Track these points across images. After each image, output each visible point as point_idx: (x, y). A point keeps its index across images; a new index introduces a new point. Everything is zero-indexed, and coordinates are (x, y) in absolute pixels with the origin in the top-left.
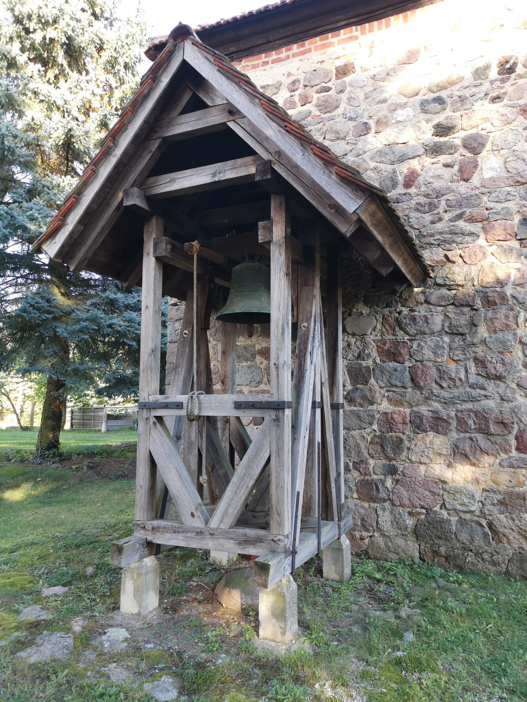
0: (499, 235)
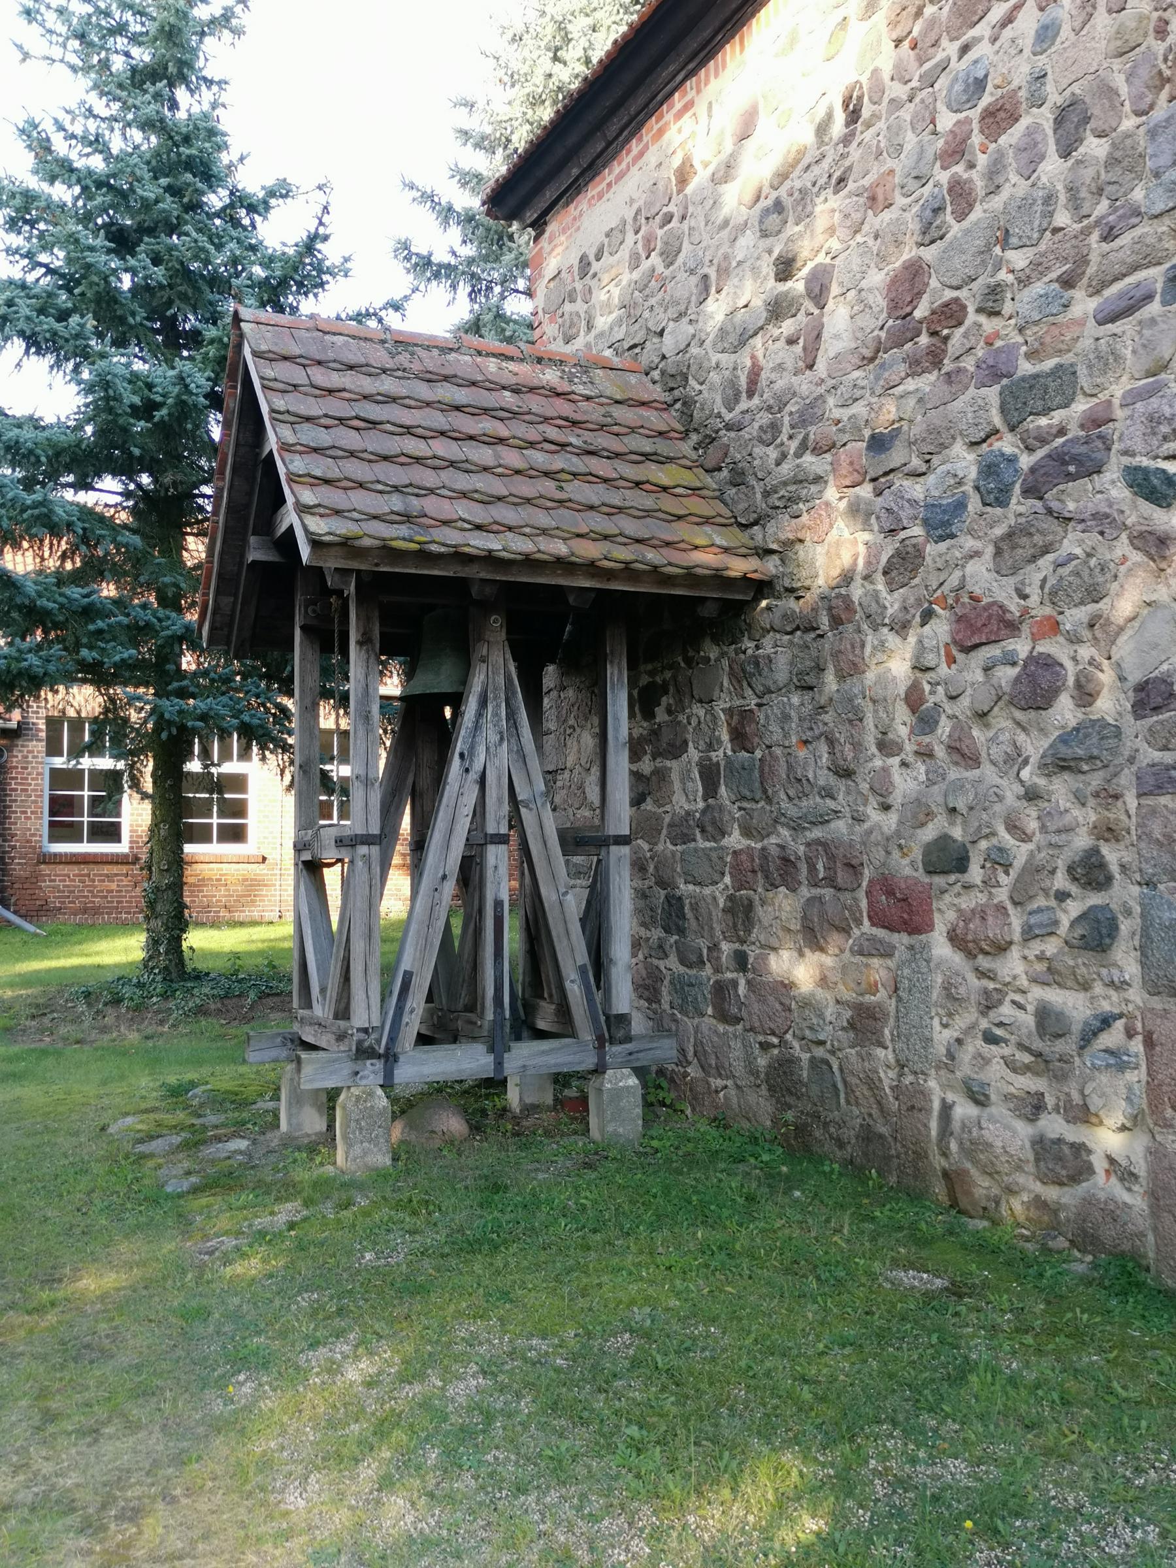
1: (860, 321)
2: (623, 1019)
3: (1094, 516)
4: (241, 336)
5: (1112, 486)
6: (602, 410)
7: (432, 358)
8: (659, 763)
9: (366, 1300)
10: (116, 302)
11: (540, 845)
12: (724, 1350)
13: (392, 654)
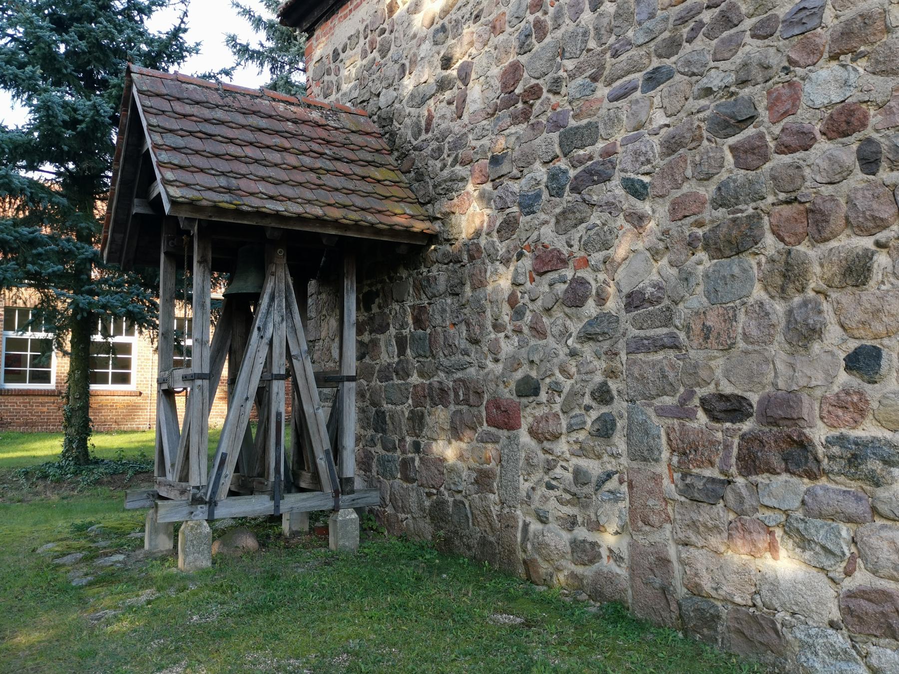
1: (486, 94)
2: (350, 481)
3: (607, 203)
4: (131, 81)
5: (615, 189)
6: (344, 136)
7: (246, 101)
8: (373, 336)
9: (193, 643)
10: (55, 59)
11: (304, 381)
12: (400, 660)
13: (220, 271)
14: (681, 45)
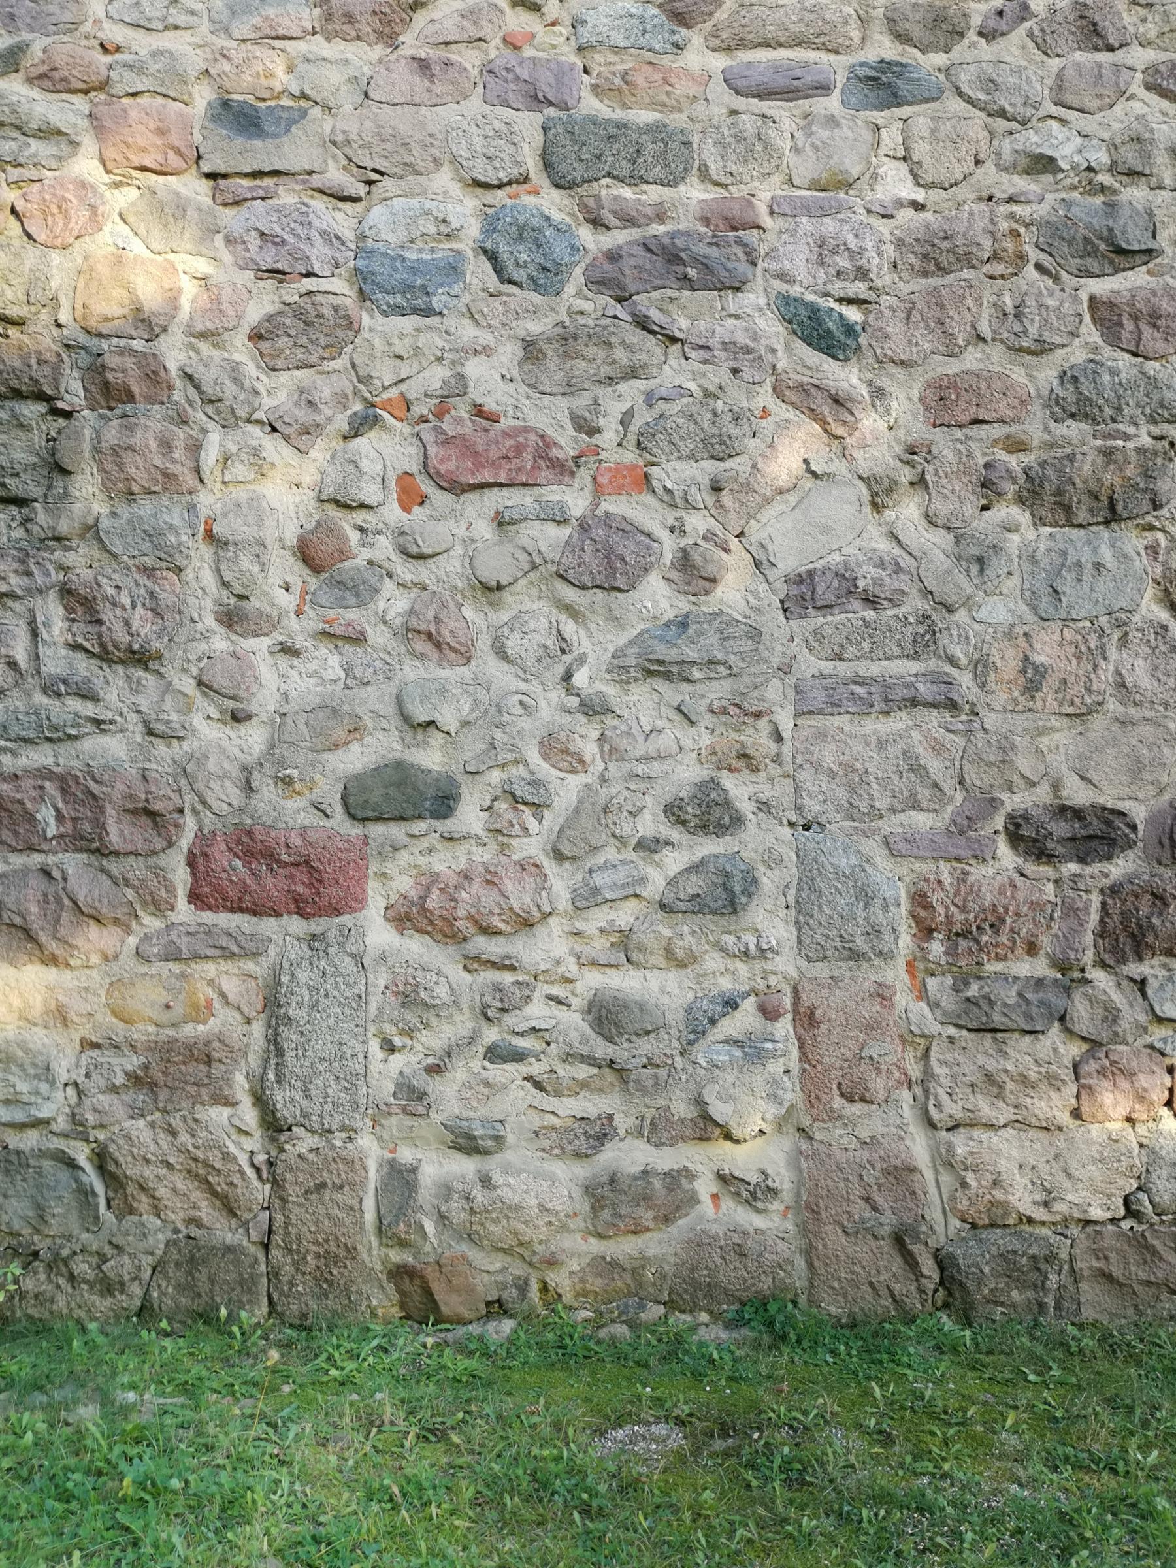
0: (144, 150)
5: (754, 314)
14: (962, 35)
